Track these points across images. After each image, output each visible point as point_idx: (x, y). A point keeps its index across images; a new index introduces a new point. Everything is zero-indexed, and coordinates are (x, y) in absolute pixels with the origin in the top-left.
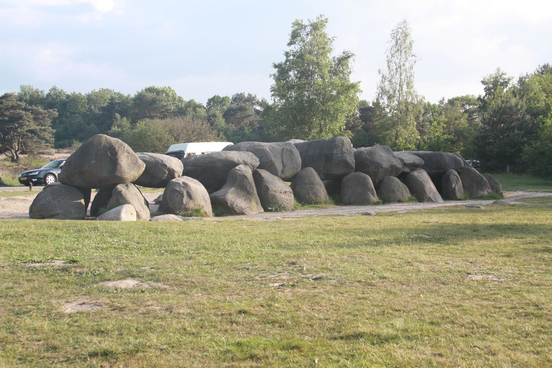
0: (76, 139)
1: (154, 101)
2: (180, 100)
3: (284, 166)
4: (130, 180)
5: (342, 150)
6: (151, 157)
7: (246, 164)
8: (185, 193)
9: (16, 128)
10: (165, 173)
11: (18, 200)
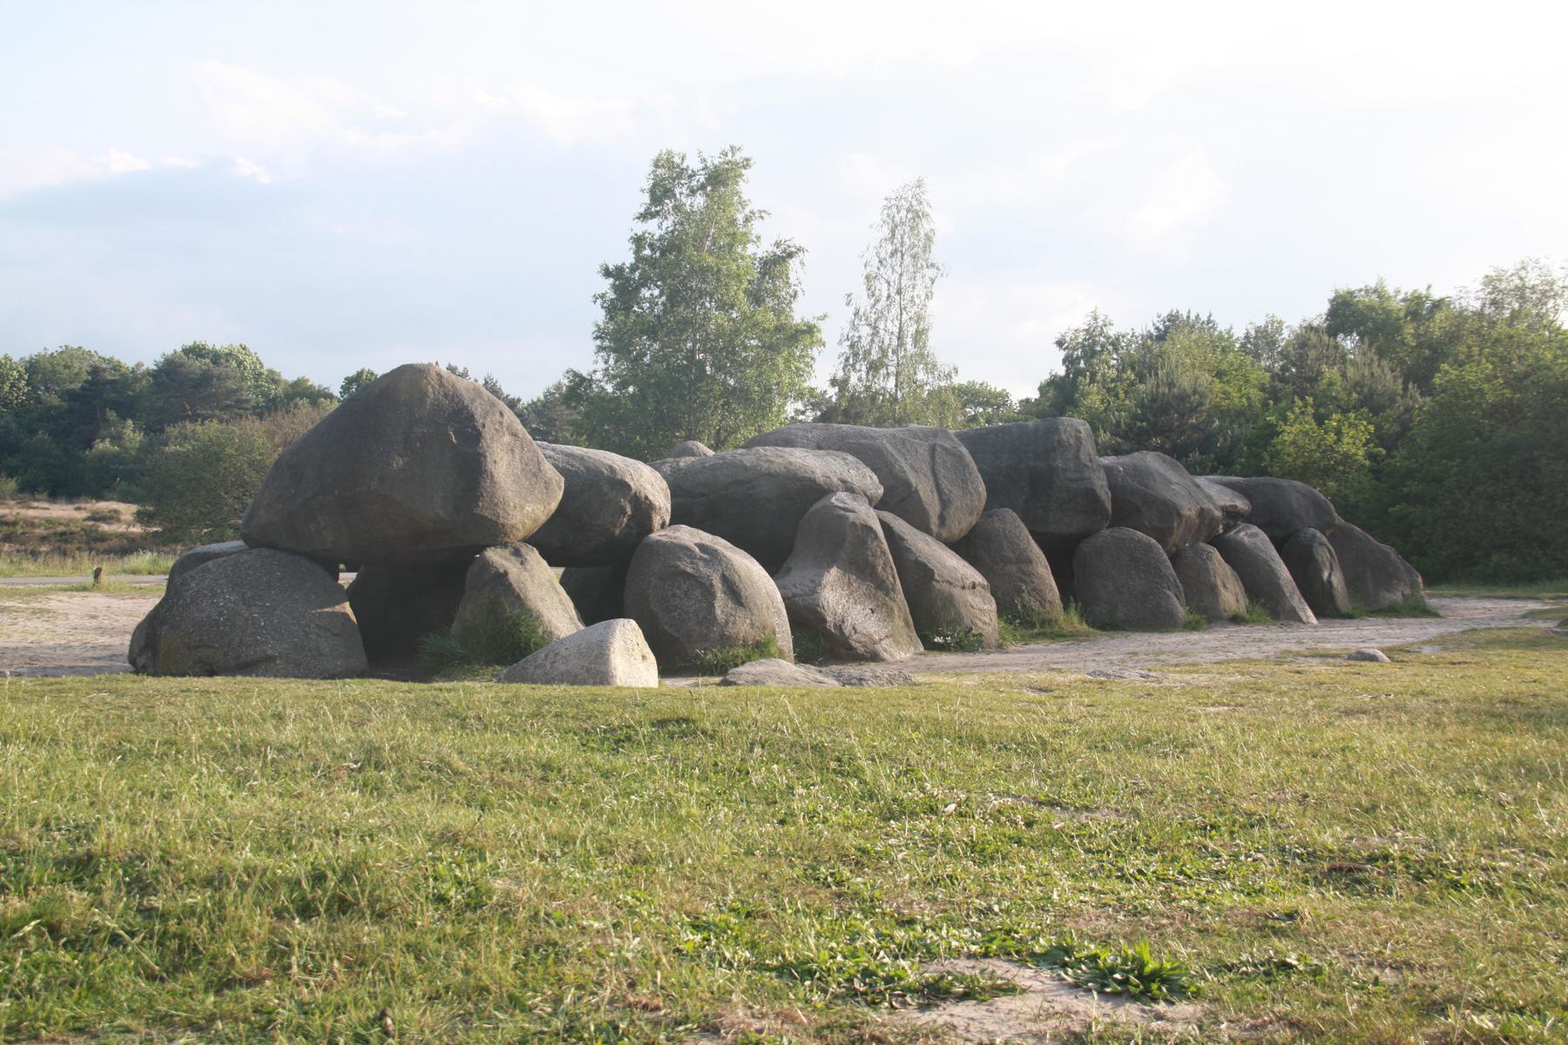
1: (205, 379)
2: (273, 378)
3: (945, 503)
4: (521, 535)
5: (1077, 457)
6: (568, 455)
7: (850, 489)
8: (718, 584)
10: (624, 513)
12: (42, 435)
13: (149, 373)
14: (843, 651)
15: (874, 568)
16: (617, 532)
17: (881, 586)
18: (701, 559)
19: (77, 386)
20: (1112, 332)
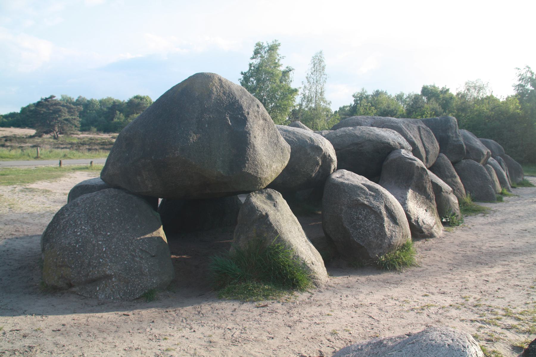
0: (93, 126)
1: (139, 104)
3: (427, 152)
8: (384, 212)
9: (57, 118)
10: (318, 164)
11: (32, 190)
12: (102, 118)
13: (126, 103)
14: (418, 234)
15: (425, 188)
16: (314, 175)
17: (428, 197)
18: (371, 195)
19: (110, 106)
20: (366, 94)
